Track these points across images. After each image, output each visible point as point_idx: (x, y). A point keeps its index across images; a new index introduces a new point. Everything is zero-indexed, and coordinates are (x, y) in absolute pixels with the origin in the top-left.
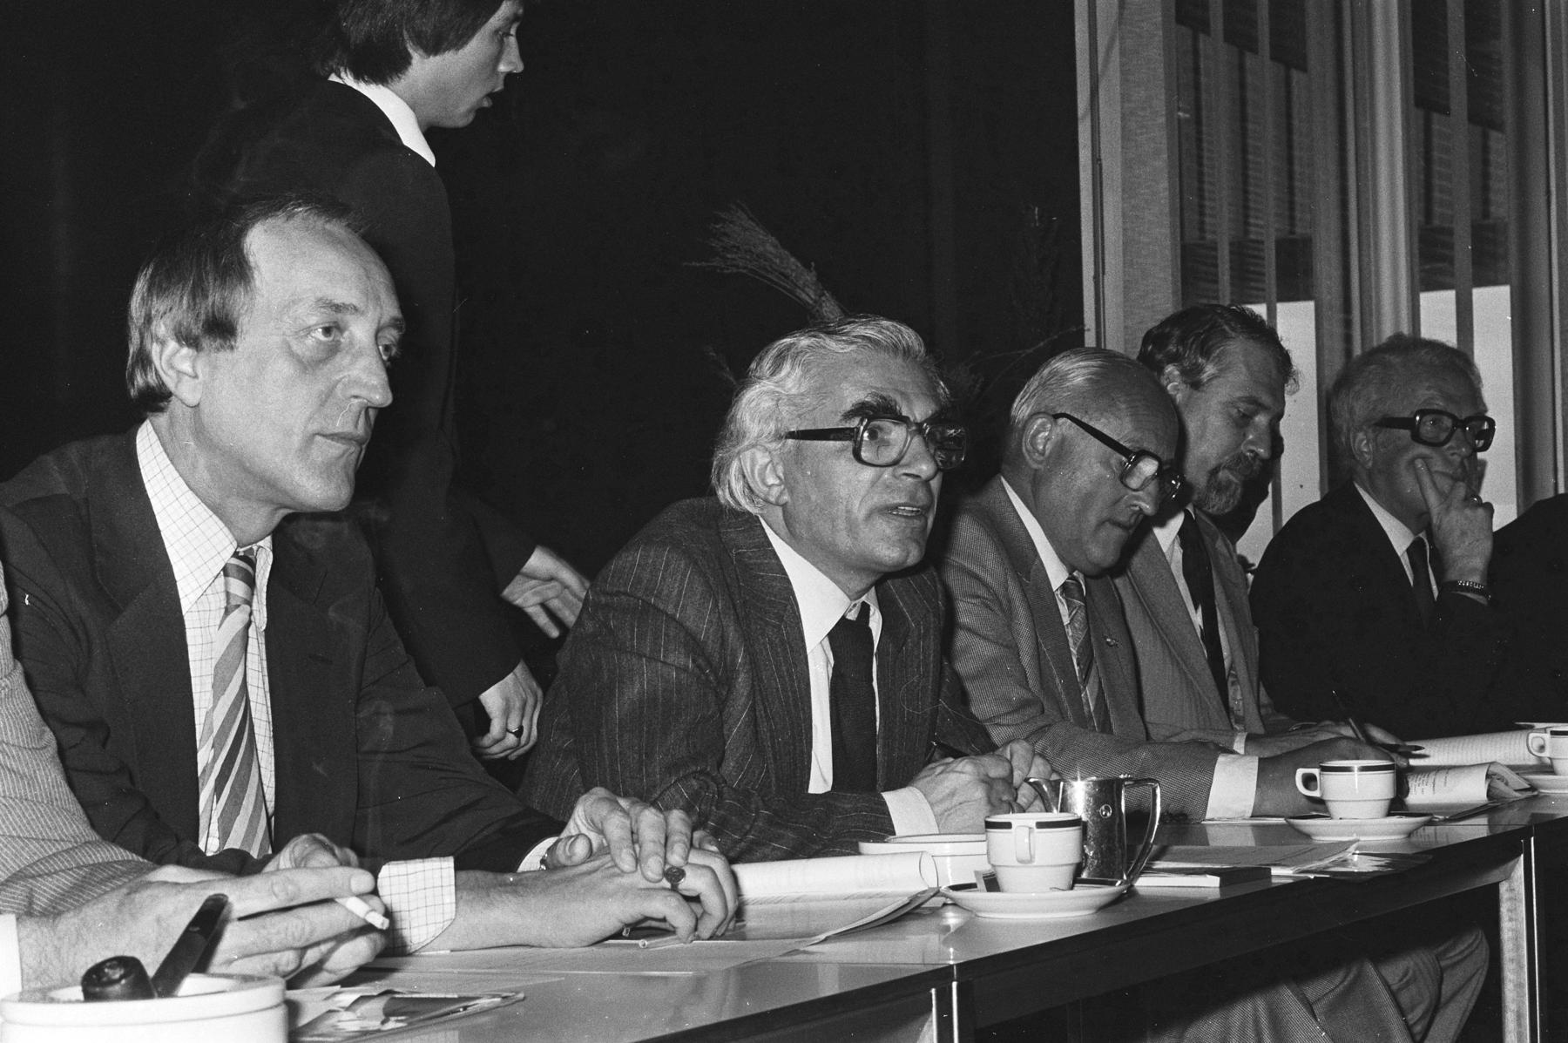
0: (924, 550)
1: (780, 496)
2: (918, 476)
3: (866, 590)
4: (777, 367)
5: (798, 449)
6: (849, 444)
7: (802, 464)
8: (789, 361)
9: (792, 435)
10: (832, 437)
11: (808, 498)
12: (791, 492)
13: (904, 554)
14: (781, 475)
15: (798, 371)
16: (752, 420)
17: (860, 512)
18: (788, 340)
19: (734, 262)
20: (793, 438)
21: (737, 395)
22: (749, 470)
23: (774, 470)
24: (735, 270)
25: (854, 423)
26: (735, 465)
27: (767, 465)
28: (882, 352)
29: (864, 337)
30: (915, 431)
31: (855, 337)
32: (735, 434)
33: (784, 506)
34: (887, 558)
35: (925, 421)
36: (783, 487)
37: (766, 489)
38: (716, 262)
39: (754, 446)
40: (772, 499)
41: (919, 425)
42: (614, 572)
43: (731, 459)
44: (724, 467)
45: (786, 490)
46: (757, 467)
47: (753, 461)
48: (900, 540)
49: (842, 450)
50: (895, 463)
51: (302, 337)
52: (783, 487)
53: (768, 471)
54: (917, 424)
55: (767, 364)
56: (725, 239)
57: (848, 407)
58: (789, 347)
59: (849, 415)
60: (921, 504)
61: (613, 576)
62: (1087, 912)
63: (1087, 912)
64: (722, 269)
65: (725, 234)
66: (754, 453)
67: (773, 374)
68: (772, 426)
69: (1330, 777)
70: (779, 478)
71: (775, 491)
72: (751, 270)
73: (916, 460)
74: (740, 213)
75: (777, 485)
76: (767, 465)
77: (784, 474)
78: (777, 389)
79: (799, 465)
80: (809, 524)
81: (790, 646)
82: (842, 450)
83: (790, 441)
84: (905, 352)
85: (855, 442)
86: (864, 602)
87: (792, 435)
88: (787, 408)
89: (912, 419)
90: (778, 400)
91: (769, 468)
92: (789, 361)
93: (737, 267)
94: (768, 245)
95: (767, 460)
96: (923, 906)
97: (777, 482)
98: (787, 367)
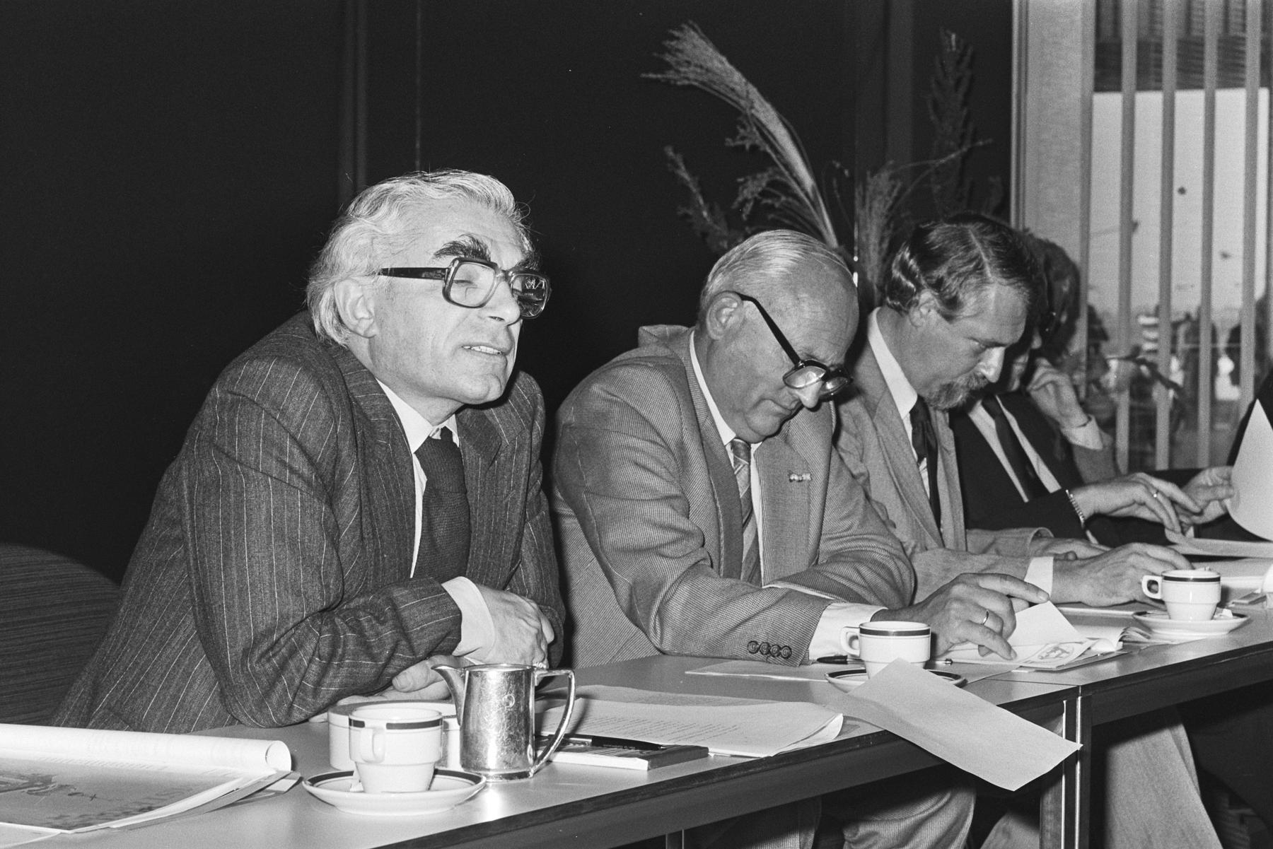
0: (503, 387)
1: (368, 329)
2: (501, 319)
3: (448, 417)
4: (374, 210)
5: (391, 286)
6: (439, 284)
7: (392, 299)
8: (387, 203)
9: (385, 272)
10: (423, 276)
11: (396, 333)
12: (381, 326)
13: (486, 388)
14: (373, 311)
15: (395, 213)
16: (348, 255)
17: (445, 348)
18: (386, 185)
19: (686, 75)
20: (385, 274)
21: (335, 231)
22: (341, 301)
23: (365, 304)
24: (686, 82)
25: (445, 262)
26: (327, 296)
27: (359, 298)
28: (476, 202)
29: (459, 187)
30: (501, 277)
31: (452, 185)
32: (329, 266)
33: (371, 338)
34: (470, 391)
35: (511, 270)
36: (372, 320)
37: (355, 322)
38: (671, 75)
39: (347, 278)
40: (361, 332)
41: (506, 272)
42: (243, 378)
43: (324, 289)
44: (318, 296)
45: (375, 324)
46: (350, 300)
47: (346, 293)
48: (482, 376)
49: (432, 290)
50: (481, 306)
51: (727, 74)
52: (372, 320)
53: (359, 305)
54: (504, 271)
55: (364, 208)
56: (680, 55)
57: (440, 246)
58: (388, 191)
59: (440, 253)
60: (500, 346)
61: (241, 380)
62: (445, 810)
63: (445, 810)
64: (675, 81)
65: (678, 50)
66: (347, 287)
67: (371, 214)
68: (365, 262)
69: (869, 639)
70: (370, 312)
71: (365, 324)
72: (703, 83)
73: (501, 304)
74: (692, 33)
75: (366, 319)
76: (359, 298)
77: (375, 308)
78: (374, 228)
79: (390, 300)
80: (396, 357)
81: (396, 463)
82: (432, 290)
83: (383, 278)
84: (496, 205)
85: (446, 281)
86: (445, 427)
87: (385, 272)
88: (381, 246)
89: (499, 266)
90: (373, 238)
91: (360, 302)
92: (387, 203)
93: (688, 79)
94: (719, 63)
95: (359, 295)
96: (268, 789)
97: (367, 316)
98: (384, 209)
